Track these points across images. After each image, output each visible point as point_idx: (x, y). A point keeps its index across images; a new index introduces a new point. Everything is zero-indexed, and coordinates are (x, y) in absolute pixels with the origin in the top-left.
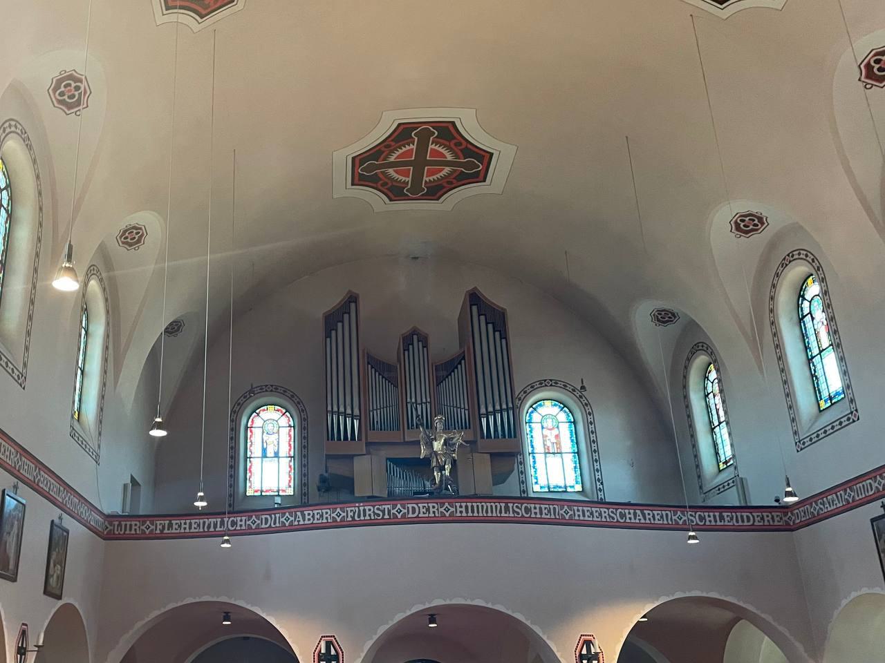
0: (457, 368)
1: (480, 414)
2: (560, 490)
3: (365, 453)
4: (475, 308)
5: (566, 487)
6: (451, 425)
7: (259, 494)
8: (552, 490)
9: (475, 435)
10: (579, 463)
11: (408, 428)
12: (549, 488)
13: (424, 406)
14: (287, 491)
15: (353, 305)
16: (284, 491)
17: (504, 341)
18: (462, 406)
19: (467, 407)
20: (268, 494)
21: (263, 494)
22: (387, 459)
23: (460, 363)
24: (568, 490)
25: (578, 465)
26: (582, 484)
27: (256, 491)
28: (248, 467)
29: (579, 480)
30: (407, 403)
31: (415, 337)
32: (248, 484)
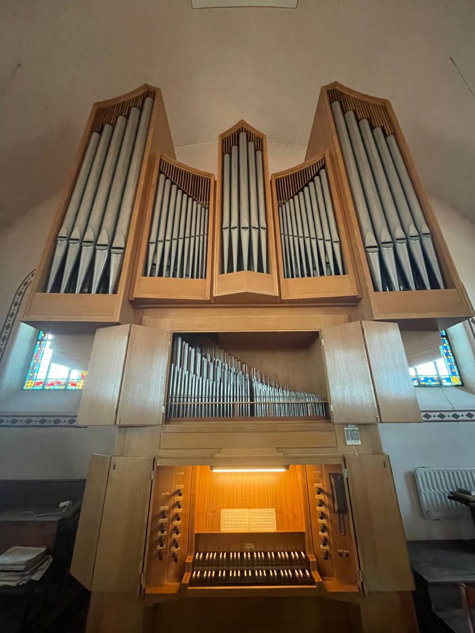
0: (312, 180)
1: (365, 248)
2: (433, 383)
3: (117, 320)
4: (337, 104)
5: (439, 380)
6: (314, 268)
7: (40, 387)
8: (423, 383)
9: (360, 286)
10: (451, 349)
11: (222, 272)
12: (419, 382)
13: (255, 233)
14: (78, 384)
15: (148, 100)
16: (74, 385)
17: (391, 138)
18: (327, 237)
19: (335, 238)
20: (52, 387)
21: (47, 387)
22: (175, 336)
23: (318, 174)
24: (444, 384)
25: (449, 351)
26: (460, 375)
27: (38, 384)
28: (35, 353)
29: (455, 370)
30: (222, 229)
31: (243, 136)
32: (30, 374)
